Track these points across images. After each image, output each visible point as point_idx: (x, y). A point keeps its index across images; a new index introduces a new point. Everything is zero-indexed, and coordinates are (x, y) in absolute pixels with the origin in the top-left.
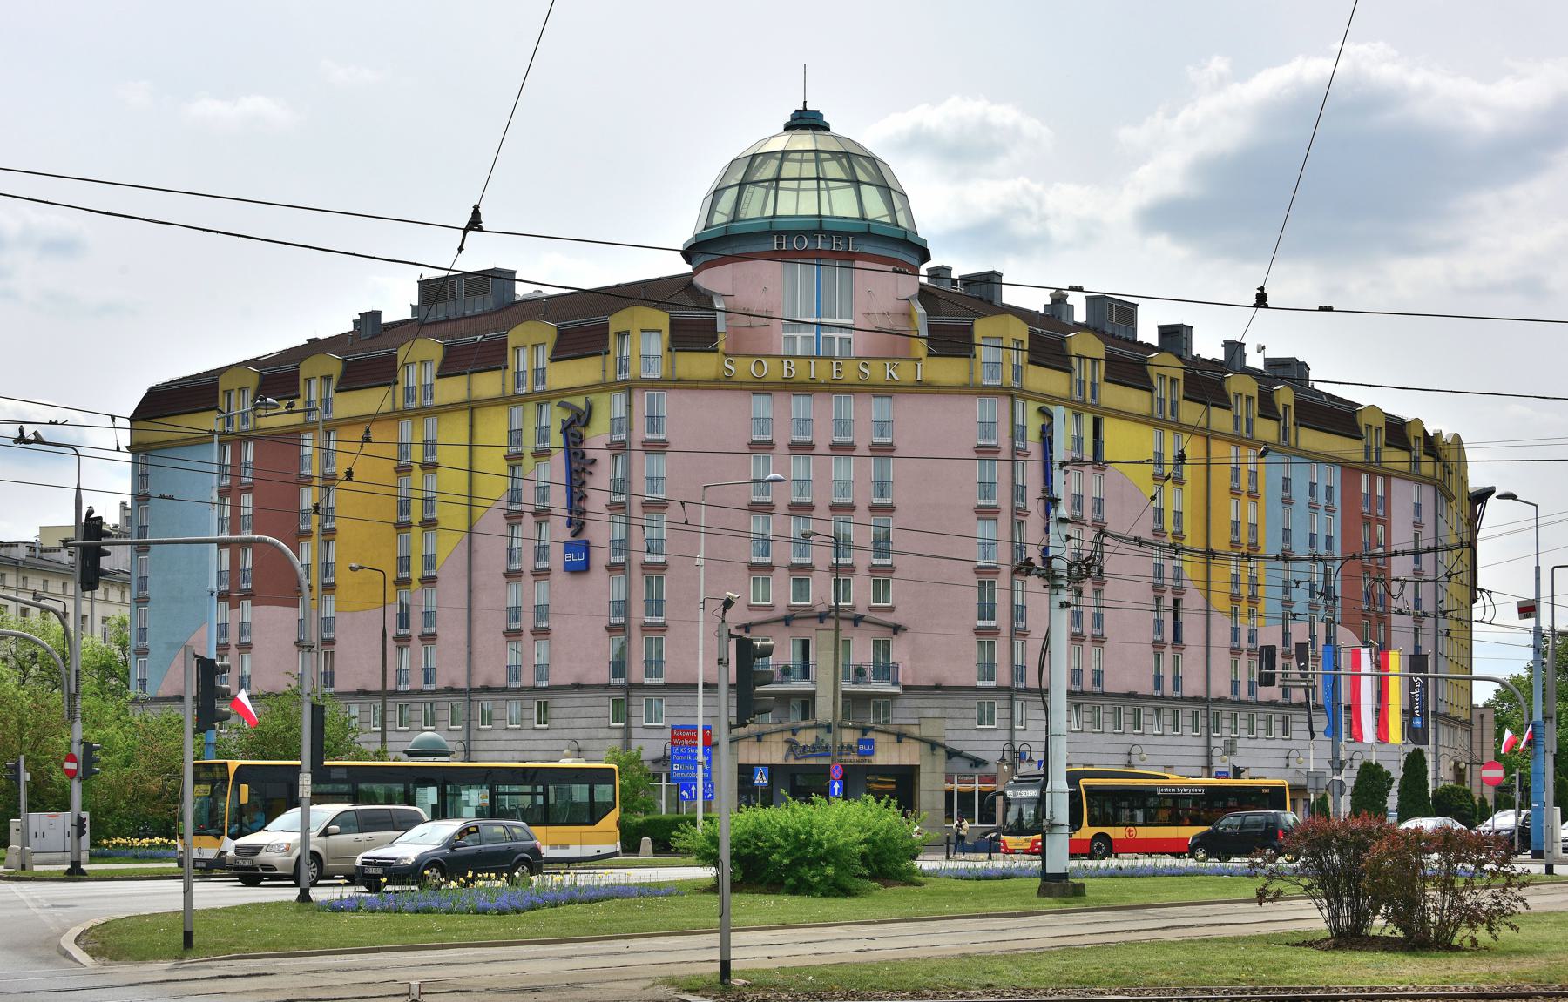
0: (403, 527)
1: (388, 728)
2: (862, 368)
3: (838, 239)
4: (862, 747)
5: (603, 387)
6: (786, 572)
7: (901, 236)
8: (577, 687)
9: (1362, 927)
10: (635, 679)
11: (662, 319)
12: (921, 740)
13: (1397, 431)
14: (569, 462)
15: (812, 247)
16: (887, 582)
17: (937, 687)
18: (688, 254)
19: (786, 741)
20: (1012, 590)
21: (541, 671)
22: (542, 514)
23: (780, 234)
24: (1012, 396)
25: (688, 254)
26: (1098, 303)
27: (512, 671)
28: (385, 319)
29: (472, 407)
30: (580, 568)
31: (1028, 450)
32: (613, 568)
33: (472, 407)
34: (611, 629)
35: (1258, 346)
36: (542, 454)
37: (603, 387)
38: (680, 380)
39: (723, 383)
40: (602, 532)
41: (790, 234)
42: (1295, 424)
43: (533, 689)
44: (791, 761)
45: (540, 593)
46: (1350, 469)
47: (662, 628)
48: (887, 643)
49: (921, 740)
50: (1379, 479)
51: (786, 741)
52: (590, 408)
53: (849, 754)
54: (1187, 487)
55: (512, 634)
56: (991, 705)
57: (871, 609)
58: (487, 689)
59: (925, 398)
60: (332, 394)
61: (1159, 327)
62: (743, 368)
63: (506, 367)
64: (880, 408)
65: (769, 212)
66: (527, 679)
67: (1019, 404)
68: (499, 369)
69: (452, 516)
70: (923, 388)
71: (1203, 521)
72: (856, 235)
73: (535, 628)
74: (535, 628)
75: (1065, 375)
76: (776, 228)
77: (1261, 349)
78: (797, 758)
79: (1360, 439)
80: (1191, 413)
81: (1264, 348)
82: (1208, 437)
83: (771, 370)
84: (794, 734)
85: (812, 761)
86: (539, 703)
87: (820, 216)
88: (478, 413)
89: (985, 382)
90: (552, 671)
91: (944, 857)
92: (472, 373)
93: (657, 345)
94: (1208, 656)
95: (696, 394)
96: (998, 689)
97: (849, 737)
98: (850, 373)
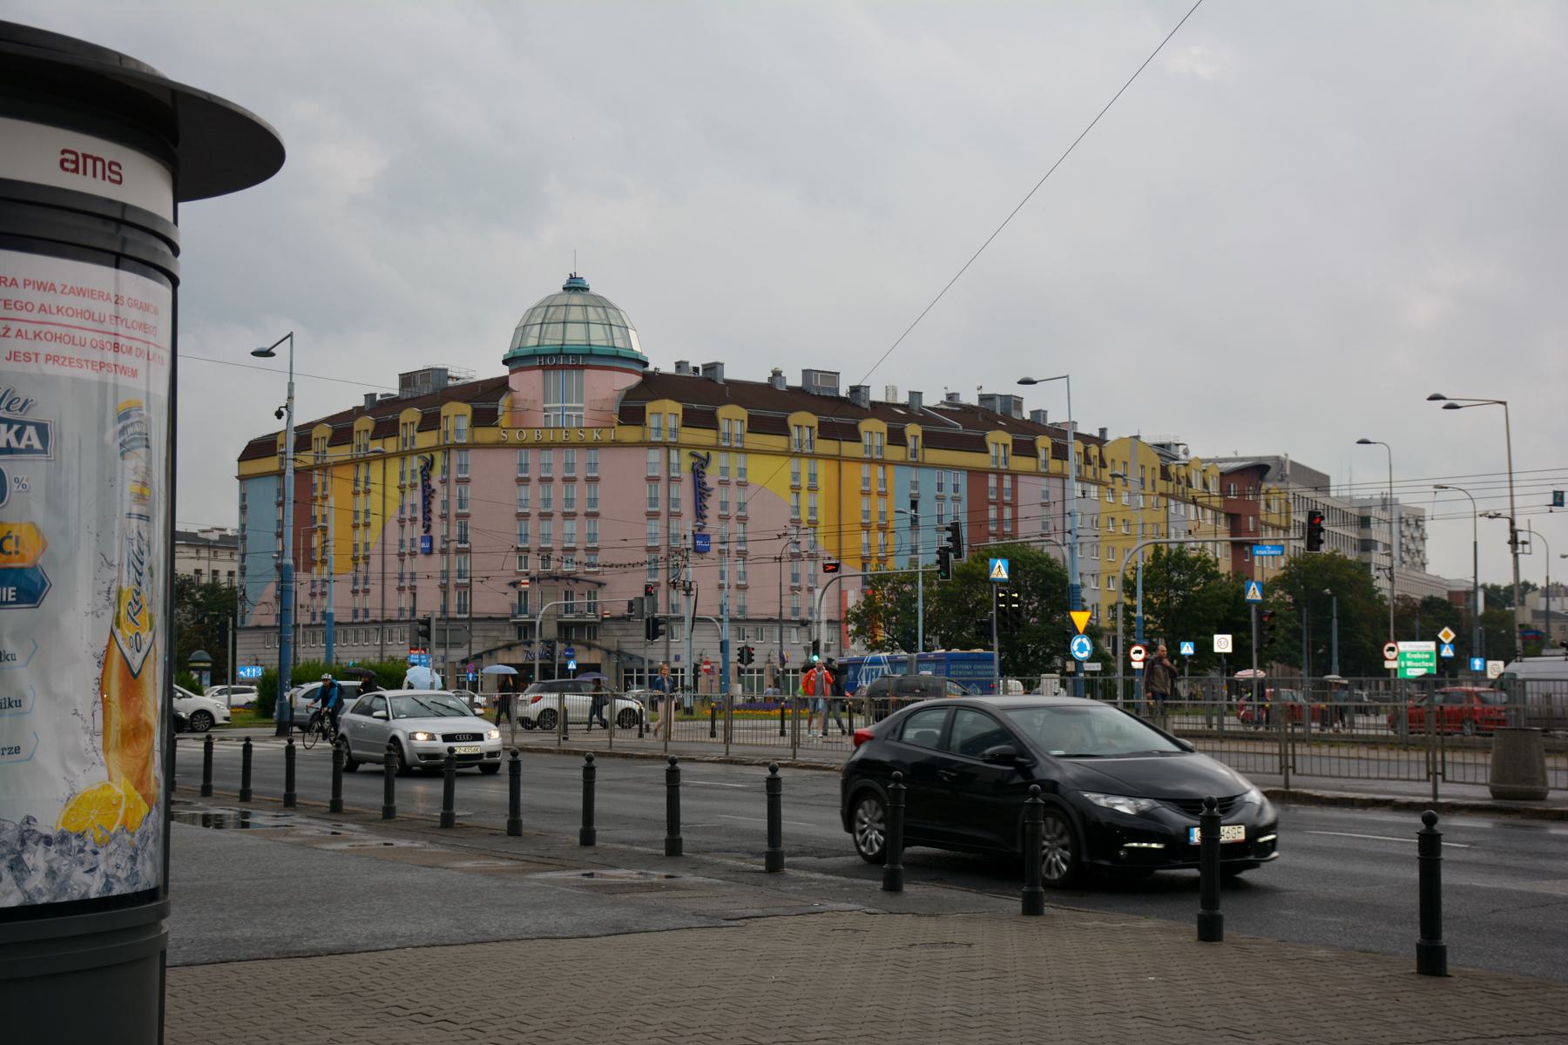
0: (355, 526)
5: (437, 448)
6: (583, 551)
7: (615, 354)
10: (451, 615)
11: (467, 409)
14: (424, 491)
15: (566, 363)
16: (526, 557)
18: (505, 362)
22: (413, 520)
23: (540, 356)
24: (667, 447)
27: (796, 611)
30: (429, 552)
32: (443, 552)
36: (413, 486)
39: (500, 445)
40: (438, 530)
41: (545, 356)
46: (977, 475)
48: (595, 593)
52: (432, 457)
54: (822, 492)
58: (390, 621)
60: (415, 433)
62: (514, 437)
64: (593, 455)
67: (674, 453)
69: (376, 522)
70: (616, 444)
80: (828, 447)
83: (533, 437)
89: (653, 439)
93: (465, 423)
94: (383, 600)
95: (486, 451)
98: (574, 438)
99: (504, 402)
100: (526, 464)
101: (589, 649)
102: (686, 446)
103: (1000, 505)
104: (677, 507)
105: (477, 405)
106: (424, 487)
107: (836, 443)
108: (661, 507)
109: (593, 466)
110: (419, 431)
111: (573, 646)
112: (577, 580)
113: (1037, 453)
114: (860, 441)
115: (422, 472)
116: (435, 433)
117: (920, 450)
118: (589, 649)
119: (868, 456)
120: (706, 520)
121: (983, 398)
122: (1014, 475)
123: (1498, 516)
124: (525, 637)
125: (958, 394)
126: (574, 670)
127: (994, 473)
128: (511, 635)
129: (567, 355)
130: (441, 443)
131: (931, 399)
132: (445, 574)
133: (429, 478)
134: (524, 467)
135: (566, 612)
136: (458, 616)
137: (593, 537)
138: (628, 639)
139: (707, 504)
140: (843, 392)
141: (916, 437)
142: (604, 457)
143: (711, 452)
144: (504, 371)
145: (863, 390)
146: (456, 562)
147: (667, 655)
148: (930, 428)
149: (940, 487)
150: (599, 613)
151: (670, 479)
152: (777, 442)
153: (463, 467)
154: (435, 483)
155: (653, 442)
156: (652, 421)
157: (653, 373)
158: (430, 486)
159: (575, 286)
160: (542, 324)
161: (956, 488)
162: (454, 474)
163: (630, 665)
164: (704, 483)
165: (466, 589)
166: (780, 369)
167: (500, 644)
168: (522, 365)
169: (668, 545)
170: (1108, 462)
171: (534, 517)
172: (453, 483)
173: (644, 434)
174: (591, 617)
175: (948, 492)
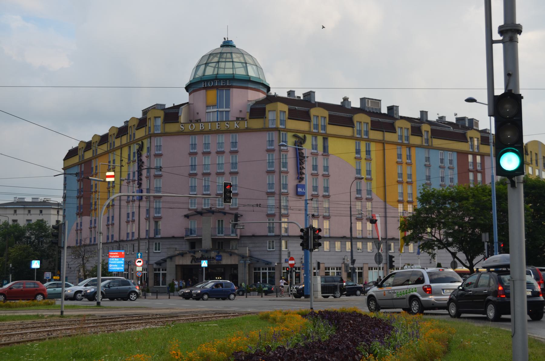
1: (147, 257)
2: (226, 124)
3: (223, 82)
4: (217, 258)
7: (248, 79)
9: (329, 321)
15: (219, 85)
19: (192, 256)
20: (280, 200)
23: (204, 81)
24: (279, 131)
29: (121, 147)
31: (288, 149)
33: (121, 147)
35: (455, 114)
37: (310, 133)
42: (431, 138)
44: (194, 263)
46: (462, 155)
47: (160, 218)
53: (213, 261)
55: (128, 222)
56: (159, 244)
57: (231, 209)
58: (123, 241)
61: (427, 112)
63: (128, 134)
65: (215, 73)
70: (248, 130)
75: (307, 123)
77: (456, 115)
78: (195, 262)
80: (376, 135)
81: (457, 114)
82: (384, 143)
86: (156, 244)
87: (233, 74)
89: (270, 126)
91: (261, 296)
93: (159, 122)
94: (120, 229)
96: (275, 236)
101: (231, 255)
102: (290, 131)
103: (475, 172)
104: (286, 168)
106: (138, 160)
107: (381, 133)
108: (275, 168)
109: (234, 144)
110: (137, 129)
112: (225, 213)
114: (395, 132)
115: (137, 152)
117: (430, 139)
118: (231, 255)
119: (400, 141)
120: (304, 176)
121: (458, 119)
124: (273, 248)
125: (445, 117)
126: (206, 268)
128: (186, 247)
131: (432, 117)
134: (194, 146)
136: (269, 234)
139: (304, 166)
140: (384, 110)
141: (428, 132)
142: (241, 138)
143: (307, 135)
144: (184, 97)
145: (395, 108)
147: (280, 259)
148: (434, 127)
149: (442, 161)
152: (346, 131)
153: (159, 147)
154: (144, 159)
156: (270, 116)
157: (274, 96)
159: (227, 44)
161: (451, 162)
162: (153, 151)
163: (258, 265)
164: (303, 154)
166: (348, 96)
167: (177, 252)
170: (529, 153)
171: (200, 176)
173: (265, 124)
175: (447, 164)
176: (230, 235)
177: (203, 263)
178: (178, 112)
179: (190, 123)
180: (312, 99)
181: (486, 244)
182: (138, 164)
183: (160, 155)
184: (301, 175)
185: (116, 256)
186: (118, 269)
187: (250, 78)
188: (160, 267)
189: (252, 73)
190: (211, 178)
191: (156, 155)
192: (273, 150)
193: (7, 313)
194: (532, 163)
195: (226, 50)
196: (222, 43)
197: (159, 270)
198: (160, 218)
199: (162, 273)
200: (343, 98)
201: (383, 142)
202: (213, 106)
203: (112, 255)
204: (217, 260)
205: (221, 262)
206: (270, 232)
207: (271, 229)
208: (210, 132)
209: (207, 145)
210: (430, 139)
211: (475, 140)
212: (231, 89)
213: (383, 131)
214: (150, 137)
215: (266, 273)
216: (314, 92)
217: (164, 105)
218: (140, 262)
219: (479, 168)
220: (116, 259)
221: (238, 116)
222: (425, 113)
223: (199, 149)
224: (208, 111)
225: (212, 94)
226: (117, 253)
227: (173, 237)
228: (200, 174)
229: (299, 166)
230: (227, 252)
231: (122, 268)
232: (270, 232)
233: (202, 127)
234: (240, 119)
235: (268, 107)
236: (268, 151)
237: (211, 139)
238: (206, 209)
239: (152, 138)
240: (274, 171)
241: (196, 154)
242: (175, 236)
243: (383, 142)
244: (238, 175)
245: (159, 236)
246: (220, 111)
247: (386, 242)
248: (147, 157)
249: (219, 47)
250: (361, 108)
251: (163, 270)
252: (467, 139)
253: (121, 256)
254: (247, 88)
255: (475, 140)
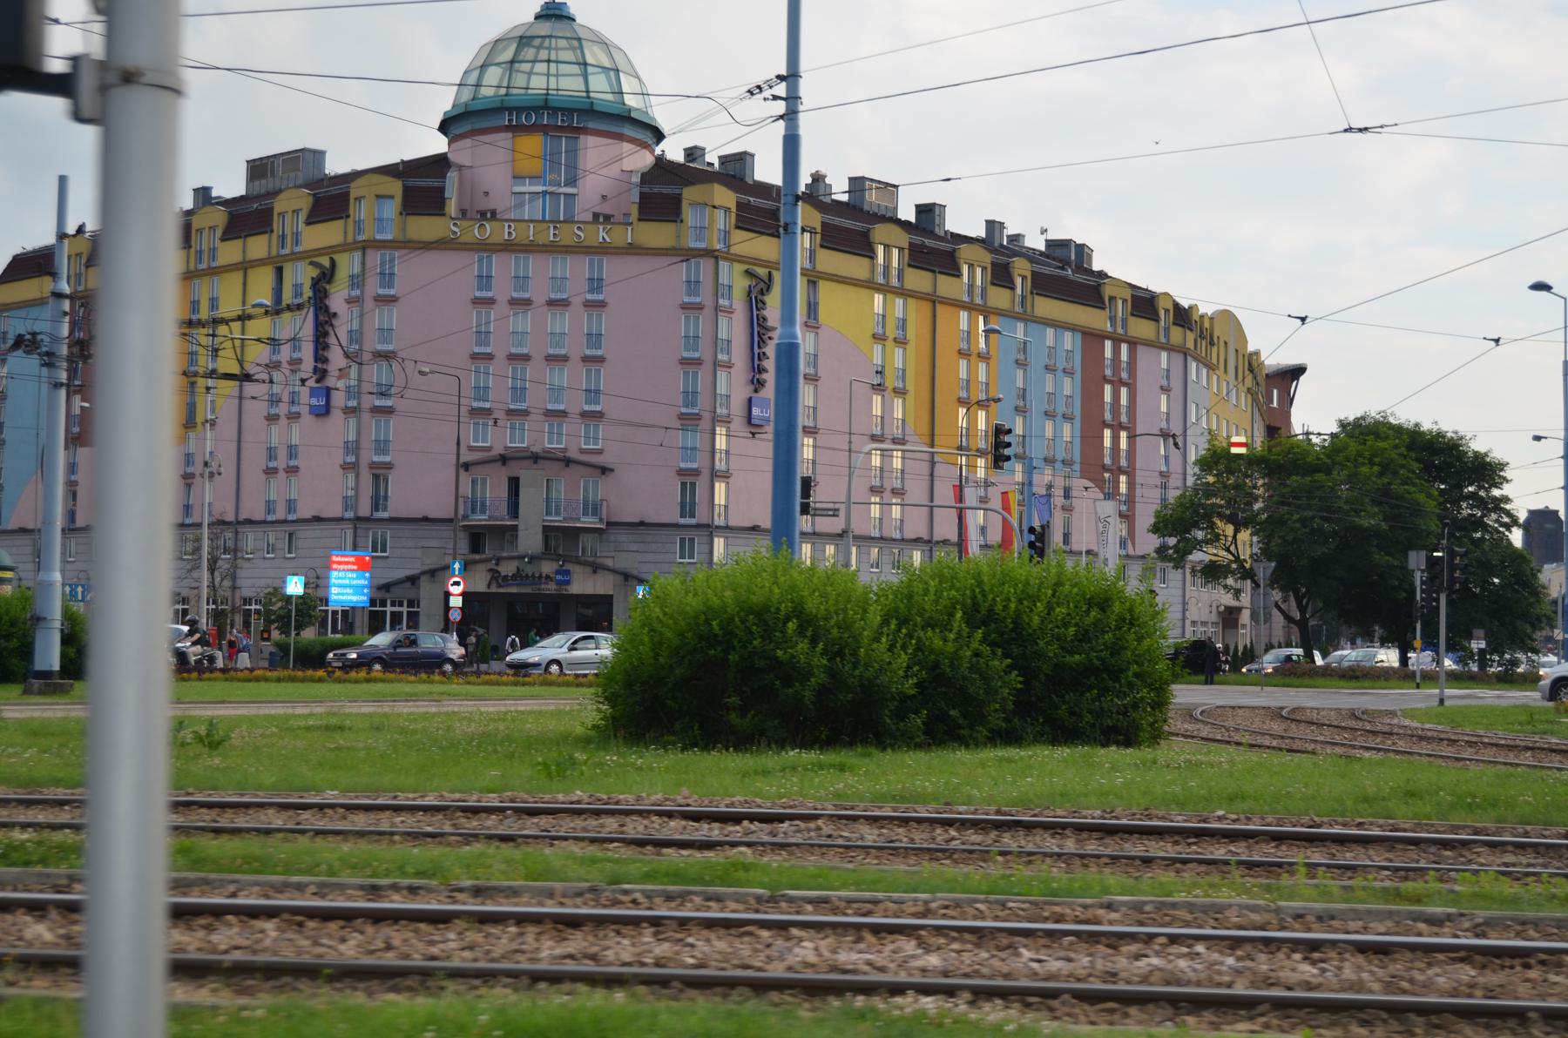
3: (563, 115)
4: (559, 577)
5: (344, 247)
8: (317, 519)
12: (614, 571)
13: (1145, 303)
15: (552, 122)
17: (642, 524)
18: (444, 127)
21: (291, 505)
23: (510, 110)
24: (716, 258)
25: (444, 127)
26: (857, 184)
27: (270, 506)
28: (214, 193)
29: (245, 266)
30: (324, 412)
32: (349, 411)
33: (245, 266)
34: (346, 467)
37: (344, 247)
38: (409, 242)
41: (519, 110)
43: (285, 521)
44: (494, 589)
45: (296, 434)
46: (1092, 338)
49: (614, 571)
50: (1124, 347)
51: (490, 570)
52: (333, 262)
54: (911, 347)
55: (270, 472)
56: (691, 540)
57: (583, 451)
58: (249, 522)
59: (635, 258)
61: (917, 206)
63: (272, 231)
66: (280, 514)
68: (265, 232)
71: (927, 379)
72: (581, 112)
73: (268, 468)
74: (268, 468)
76: (506, 105)
77: (1044, 231)
78: (500, 586)
79: (1104, 309)
80: (918, 280)
82: (934, 302)
84: (497, 564)
85: (514, 590)
86: (682, 540)
88: (251, 272)
89: (692, 245)
90: (299, 506)
92: (246, 236)
93: (391, 209)
96: (698, 526)
97: (547, 568)
99: (452, 175)
100: (489, 277)
105: (412, 182)
107: (929, 275)
108: (703, 352)
109: (596, 284)
111: (568, 566)
113: (1158, 315)
116: (339, 224)
120: (765, 376)
122: (1133, 344)
123: (754, 528)
124: (692, 557)
127: (1109, 338)
129: (554, 110)
130: (350, 239)
132: (353, 448)
133: (326, 294)
134: (485, 280)
135: (585, 513)
136: (682, 521)
137: (593, 394)
138: (650, 557)
140: (907, 213)
142: (611, 268)
144: (438, 144)
145: (937, 210)
146: (372, 428)
150: (604, 516)
151: (717, 309)
153: (387, 278)
154: (337, 302)
155: (692, 249)
156: (689, 215)
158: (327, 309)
160: (512, 62)
162: (373, 287)
164: (765, 319)
165: (380, 474)
166: (823, 171)
168: (478, 125)
169: (715, 412)
172: (369, 303)
174: (588, 521)
176: (578, 519)
177: (293, 584)
178: (444, 188)
179: (479, 220)
180: (747, 172)
181: (1418, 575)
182: (316, 316)
183: (392, 300)
184: (760, 373)
185: (350, 567)
186: (355, 598)
187: (630, 111)
188: (387, 595)
189: (599, 86)
190: (530, 370)
191: (381, 300)
192: (699, 307)
193: (69, 710)
194: (1218, 368)
195: (545, 28)
196: (538, 9)
197: (383, 604)
198: (389, 466)
199: (392, 613)
200: (812, 175)
201: (933, 300)
202: (534, 178)
203: (340, 563)
204: (559, 583)
205: (569, 587)
206: (683, 515)
207: (687, 508)
208: (530, 248)
209: (521, 281)
210: (1029, 297)
211: (1120, 303)
212: (582, 137)
213: (934, 272)
214: (364, 249)
215: (401, 613)
216: (752, 156)
217: (318, 155)
218: (457, 583)
219: (1124, 375)
220: (349, 575)
221: (597, 210)
222: (997, 226)
223: (502, 290)
224: (517, 189)
225: (532, 144)
226: (352, 559)
227: (426, 519)
228: (501, 355)
229: (756, 350)
230: (585, 564)
231: (365, 598)
232: (683, 515)
233: (510, 233)
234: (601, 219)
235: (689, 194)
236: (685, 307)
237: (534, 265)
238: (518, 450)
239: (369, 252)
240: (699, 359)
241: (490, 302)
242: (431, 516)
243: (933, 300)
244: (605, 364)
245: (385, 515)
246: (550, 193)
247: (931, 551)
248: (350, 301)
249: (532, 19)
250: (852, 202)
251: (393, 604)
252: (1103, 303)
253: (362, 566)
254: (620, 137)
255: (1120, 303)
